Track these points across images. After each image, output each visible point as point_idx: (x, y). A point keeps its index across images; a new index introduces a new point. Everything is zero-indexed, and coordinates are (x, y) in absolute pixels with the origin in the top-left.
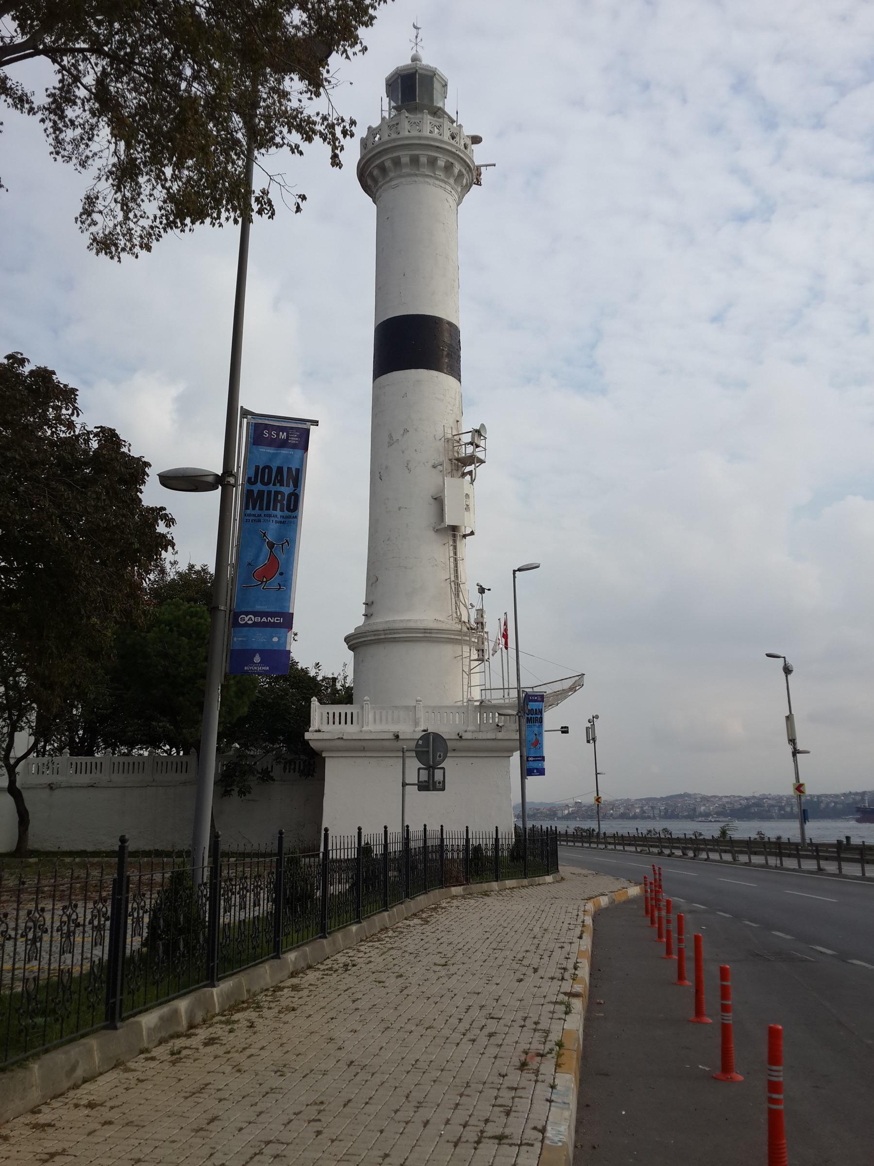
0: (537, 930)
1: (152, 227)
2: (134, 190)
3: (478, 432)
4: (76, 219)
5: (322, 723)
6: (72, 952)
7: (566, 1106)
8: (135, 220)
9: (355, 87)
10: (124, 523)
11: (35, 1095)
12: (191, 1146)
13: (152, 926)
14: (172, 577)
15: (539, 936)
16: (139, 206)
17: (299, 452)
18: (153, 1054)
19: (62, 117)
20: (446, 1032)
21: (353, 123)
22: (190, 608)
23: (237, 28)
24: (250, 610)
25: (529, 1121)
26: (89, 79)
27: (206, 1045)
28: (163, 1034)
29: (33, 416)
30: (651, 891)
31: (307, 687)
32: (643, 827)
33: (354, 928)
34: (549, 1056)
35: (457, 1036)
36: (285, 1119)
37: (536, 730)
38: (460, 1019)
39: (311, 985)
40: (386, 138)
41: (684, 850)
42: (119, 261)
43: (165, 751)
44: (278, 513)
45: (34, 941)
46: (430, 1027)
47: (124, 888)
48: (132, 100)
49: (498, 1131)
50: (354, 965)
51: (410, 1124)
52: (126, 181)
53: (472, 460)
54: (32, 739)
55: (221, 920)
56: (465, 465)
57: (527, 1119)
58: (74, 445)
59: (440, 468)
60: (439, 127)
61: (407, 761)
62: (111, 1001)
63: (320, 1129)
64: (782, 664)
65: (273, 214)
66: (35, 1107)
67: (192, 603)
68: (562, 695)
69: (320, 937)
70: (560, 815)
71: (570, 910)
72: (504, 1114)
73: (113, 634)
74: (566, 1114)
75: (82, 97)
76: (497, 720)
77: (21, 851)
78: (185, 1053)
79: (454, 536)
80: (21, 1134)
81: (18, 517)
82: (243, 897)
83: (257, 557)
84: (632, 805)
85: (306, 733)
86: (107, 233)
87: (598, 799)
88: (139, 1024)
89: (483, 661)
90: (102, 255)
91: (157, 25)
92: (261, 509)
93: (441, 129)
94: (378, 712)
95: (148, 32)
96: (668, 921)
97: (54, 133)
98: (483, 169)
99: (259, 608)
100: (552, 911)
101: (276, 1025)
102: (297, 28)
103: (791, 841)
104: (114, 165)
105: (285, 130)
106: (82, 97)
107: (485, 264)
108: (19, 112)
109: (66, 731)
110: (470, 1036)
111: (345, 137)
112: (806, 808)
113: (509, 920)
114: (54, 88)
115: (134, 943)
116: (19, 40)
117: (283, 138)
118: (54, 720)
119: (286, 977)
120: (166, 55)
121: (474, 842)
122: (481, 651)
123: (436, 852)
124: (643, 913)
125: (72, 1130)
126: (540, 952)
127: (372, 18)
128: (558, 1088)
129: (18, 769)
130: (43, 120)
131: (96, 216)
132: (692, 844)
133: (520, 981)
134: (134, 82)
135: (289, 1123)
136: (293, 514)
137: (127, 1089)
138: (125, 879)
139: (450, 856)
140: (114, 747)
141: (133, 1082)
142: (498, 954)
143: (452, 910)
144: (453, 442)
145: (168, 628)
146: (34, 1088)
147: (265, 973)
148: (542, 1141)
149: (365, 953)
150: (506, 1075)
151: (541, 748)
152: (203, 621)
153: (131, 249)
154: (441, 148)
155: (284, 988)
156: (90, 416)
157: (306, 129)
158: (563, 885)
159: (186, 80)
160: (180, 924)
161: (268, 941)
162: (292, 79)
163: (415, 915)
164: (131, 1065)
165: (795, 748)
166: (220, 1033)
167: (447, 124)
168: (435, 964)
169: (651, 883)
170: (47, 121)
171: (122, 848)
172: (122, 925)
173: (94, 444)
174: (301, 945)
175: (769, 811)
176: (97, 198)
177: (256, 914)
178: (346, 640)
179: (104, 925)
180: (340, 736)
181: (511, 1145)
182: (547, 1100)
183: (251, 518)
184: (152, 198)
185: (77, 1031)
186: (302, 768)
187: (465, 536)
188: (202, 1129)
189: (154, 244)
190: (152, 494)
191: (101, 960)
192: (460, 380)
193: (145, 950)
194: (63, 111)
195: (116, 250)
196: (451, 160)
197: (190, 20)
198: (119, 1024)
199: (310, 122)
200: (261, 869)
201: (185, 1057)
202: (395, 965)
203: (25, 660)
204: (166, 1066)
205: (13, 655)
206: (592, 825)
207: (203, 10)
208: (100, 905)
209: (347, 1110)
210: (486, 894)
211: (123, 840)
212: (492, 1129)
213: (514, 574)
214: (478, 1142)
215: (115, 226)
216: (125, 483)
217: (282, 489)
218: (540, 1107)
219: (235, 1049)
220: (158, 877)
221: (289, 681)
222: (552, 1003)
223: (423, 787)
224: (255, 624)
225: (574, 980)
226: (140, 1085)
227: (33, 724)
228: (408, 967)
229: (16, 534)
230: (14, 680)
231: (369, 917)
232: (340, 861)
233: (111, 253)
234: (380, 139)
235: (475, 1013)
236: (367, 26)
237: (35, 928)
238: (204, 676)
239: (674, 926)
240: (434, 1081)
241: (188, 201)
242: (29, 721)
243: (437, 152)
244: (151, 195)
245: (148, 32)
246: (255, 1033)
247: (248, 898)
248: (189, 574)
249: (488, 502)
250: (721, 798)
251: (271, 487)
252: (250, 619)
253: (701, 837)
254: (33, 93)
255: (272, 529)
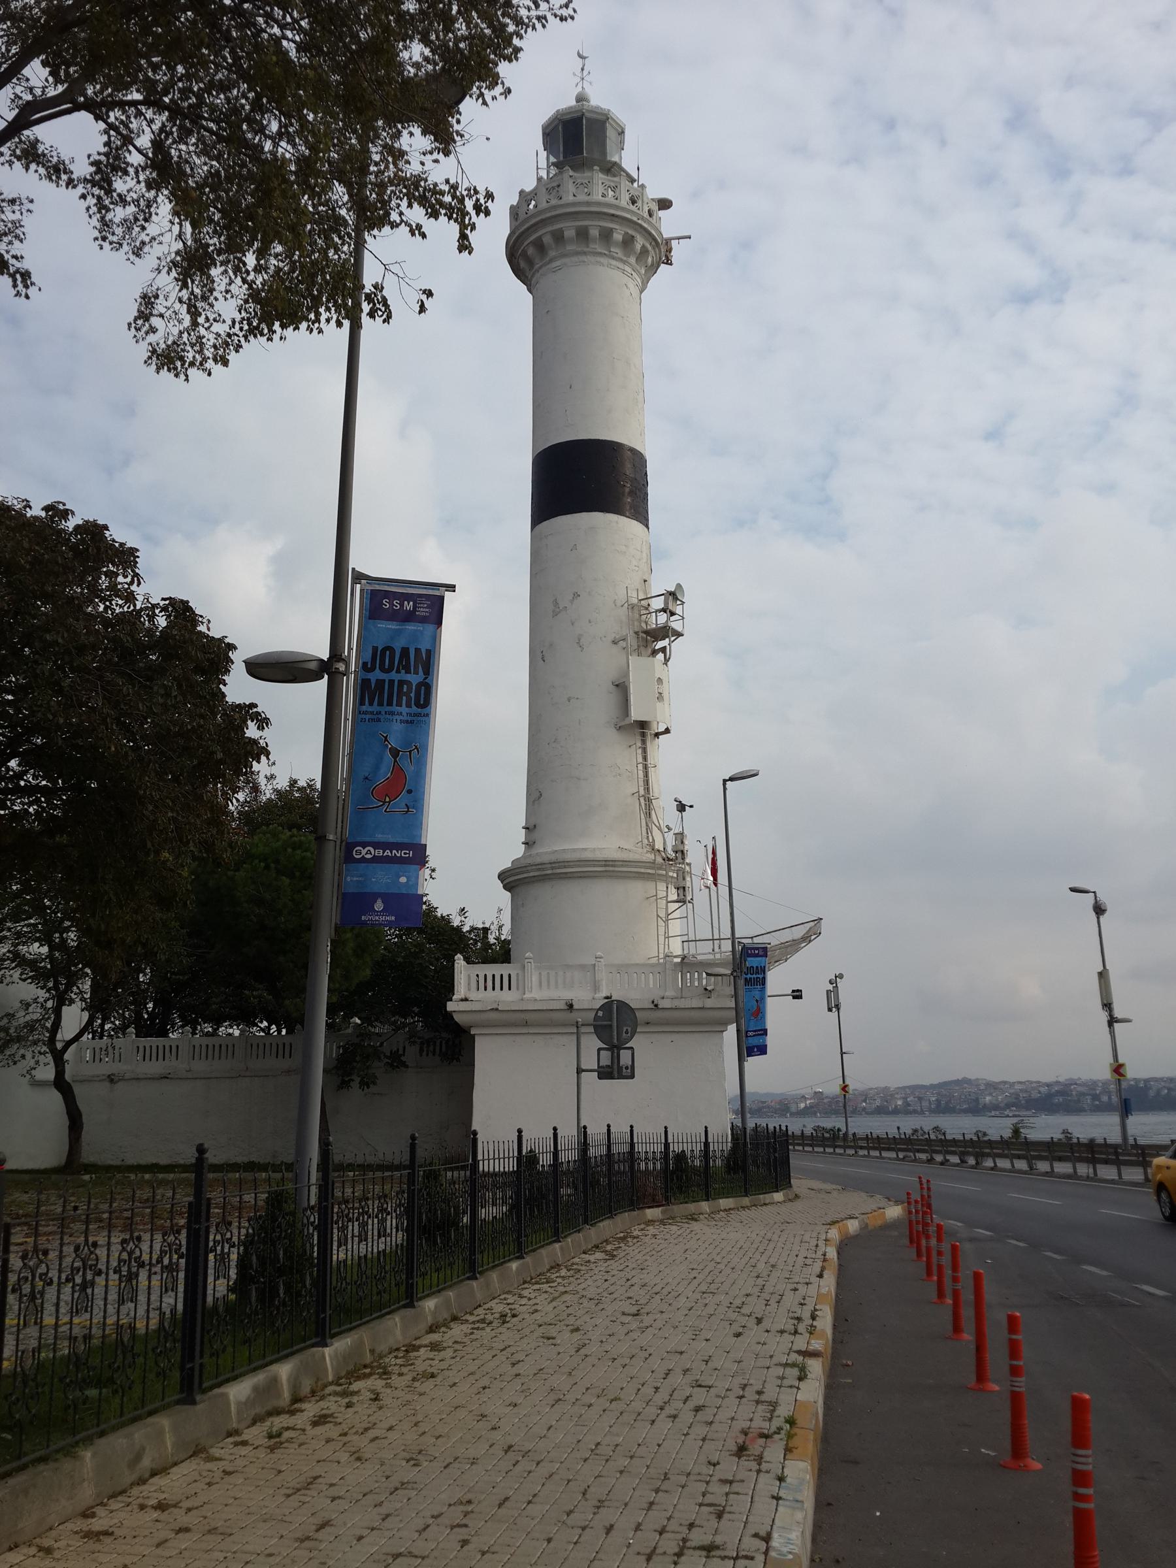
0: (761, 1266)
1: (229, 335)
2: (205, 286)
3: (672, 595)
4: (129, 325)
5: (470, 988)
6: (134, 1299)
7: (799, 1505)
8: (207, 325)
9: (498, 144)
10: (202, 726)
11: (87, 1494)
12: (293, 1561)
13: (243, 1264)
14: (268, 796)
15: (765, 1274)
16: (212, 306)
17: (430, 628)
18: (245, 1437)
19: (109, 191)
20: (638, 1405)
21: (490, 196)
22: (291, 836)
23: (337, 68)
24: (368, 839)
25: (748, 1526)
26: (144, 141)
27: (315, 1424)
28: (259, 1410)
29: (81, 586)
30: (917, 1212)
31: (448, 940)
32: (907, 1125)
33: (514, 1265)
34: (776, 1437)
35: (652, 1411)
36: (419, 1523)
37: (757, 994)
38: (657, 1388)
39: (456, 1342)
40: (543, 205)
41: (962, 1155)
42: (187, 380)
43: (262, 1030)
44: (404, 709)
45: (84, 1285)
46: (615, 1399)
47: (204, 1214)
48: (201, 166)
49: (707, 1540)
50: (514, 1316)
51: (588, 1530)
52: (194, 273)
53: (665, 632)
54: (86, 1016)
55: (335, 1257)
56: (657, 640)
57: (746, 1523)
58: (135, 624)
59: (623, 644)
60: (614, 189)
61: (583, 1039)
62: (188, 1366)
63: (466, 1537)
64: (1093, 902)
65: (389, 317)
66: (88, 1509)
67: (295, 831)
68: (792, 947)
69: (469, 1279)
70: (793, 1109)
71: (806, 1238)
72: (714, 1516)
73: (192, 873)
74: (799, 1516)
75: (135, 164)
76: (704, 982)
77: (72, 1164)
78: (287, 1435)
79: (643, 735)
80: (68, 1545)
81: (61, 721)
82: (363, 1225)
83: (377, 767)
84: (892, 1095)
85: (449, 1003)
86: (169, 343)
87: (844, 1088)
88: (225, 1396)
89: (684, 902)
90: (164, 372)
91: (231, 65)
92: (381, 704)
93: (617, 191)
94: (544, 973)
95: (220, 76)
96: (940, 1253)
97: (99, 212)
98: (674, 243)
99: (380, 837)
100: (782, 1239)
101: (409, 1397)
102: (417, 65)
103: (1109, 1141)
104: (178, 253)
105: (404, 203)
106: (135, 164)
107: (678, 366)
108: (54, 185)
109: (132, 1003)
110: (669, 1410)
111: (478, 215)
112: (1128, 1097)
113: (724, 1253)
114: (99, 154)
115: (218, 1288)
116: (51, 92)
117: (401, 214)
118: (115, 990)
119: (423, 1332)
120: (243, 106)
121: (675, 1148)
122: (682, 889)
123: (624, 1161)
124: (906, 1241)
125: (137, 1540)
126: (766, 1296)
127: (517, 50)
128: (789, 1480)
129: (66, 1056)
130: (83, 197)
131: (155, 321)
132: (973, 1147)
133: (738, 1335)
134: (204, 143)
135: (424, 1529)
136: (424, 711)
137: (209, 1484)
138: (204, 1202)
139: (643, 1166)
140: (194, 1024)
141: (218, 1474)
142: (709, 1299)
143: (646, 1239)
144: (640, 608)
145: (262, 864)
146: (86, 1484)
147: (395, 1328)
148: (766, 1553)
149: (530, 1299)
150: (718, 1463)
151: (763, 1018)
152: (308, 854)
153: (201, 364)
154: (617, 216)
155: (420, 1346)
156: (154, 586)
157: (430, 199)
158: (798, 1205)
159: (270, 137)
160: (279, 1261)
161: (397, 1284)
162: (411, 134)
163: (597, 1247)
164: (216, 1452)
165: (1111, 1016)
166: (333, 1408)
167: (625, 184)
168: (624, 1314)
169: (916, 1202)
170: (89, 198)
171: (200, 1159)
172: (201, 1264)
173: (162, 622)
174: (443, 1289)
175: (1079, 1101)
176: (157, 297)
177: (382, 1247)
178: (499, 877)
179: (177, 1264)
180: (495, 1006)
181: (723, 1558)
182: (773, 1497)
183: (367, 717)
184: (228, 296)
185: (143, 1407)
186: (444, 1049)
187: (657, 735)
188: (308, 1538)
189: (232, 356)
190: (238, 687)
191: (174, 1311)
192: (647, 526)
193: (232, 1297)
194: (110, 183)
195: (182, 365)
196: (631, 232)
197: (274, 58)
198: (198, 1398)
199: (435, 191)
200: (387, 1187)
201: (287, 1441)
202: (569, 1315)
203: (75, 911)
204: (261, 1453)
205: (59, 903)
206: (837, 1122)
207: (293, 45)
208: (172, 1238)
209: (503, 1511)
210: (693, 1218)
211: (201, 1150)
212: (698, 1537)
213: (724, 784)
214: (679, 1555)
215: (181, 333)
216: (203, 672)
217: (409, 677)
218: (764, 1506)
219: (354, 1430)
220: (249, 1198)
221: (425, 933)
222: (781, 1365)
223: (605, 1073)
224: (375, 860)
225: (811, 1333)
226: (227, 1478)
227: (87, 996)
228: (587, 1318)
229: (60, 742)
230: (61, 937)
231: (534, 1251)
232: (495, 1174)
233: (175, 369)
234: (536, 206)
235: (677, 1379)
236: (510, 61)
237: (85, 1270)
238: (309, 928)
239: (946, 1260)
240: (621, 1472)
241: (276, 298)
242: (81, 992)
243: (612, 221)
244: (227, 292)
245: (220, 76)
246: (381, 1408)
247: (370, 1227)
248: (290, 792)
249: (689, 689)
250: (1012, 1084)
251: (394, 675)
252: (369, 852)
253: (986, 1138)
254: (72, 160)
255: (395, 731)
